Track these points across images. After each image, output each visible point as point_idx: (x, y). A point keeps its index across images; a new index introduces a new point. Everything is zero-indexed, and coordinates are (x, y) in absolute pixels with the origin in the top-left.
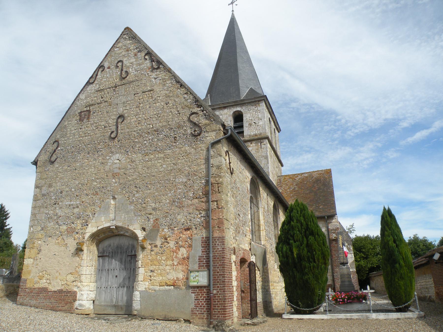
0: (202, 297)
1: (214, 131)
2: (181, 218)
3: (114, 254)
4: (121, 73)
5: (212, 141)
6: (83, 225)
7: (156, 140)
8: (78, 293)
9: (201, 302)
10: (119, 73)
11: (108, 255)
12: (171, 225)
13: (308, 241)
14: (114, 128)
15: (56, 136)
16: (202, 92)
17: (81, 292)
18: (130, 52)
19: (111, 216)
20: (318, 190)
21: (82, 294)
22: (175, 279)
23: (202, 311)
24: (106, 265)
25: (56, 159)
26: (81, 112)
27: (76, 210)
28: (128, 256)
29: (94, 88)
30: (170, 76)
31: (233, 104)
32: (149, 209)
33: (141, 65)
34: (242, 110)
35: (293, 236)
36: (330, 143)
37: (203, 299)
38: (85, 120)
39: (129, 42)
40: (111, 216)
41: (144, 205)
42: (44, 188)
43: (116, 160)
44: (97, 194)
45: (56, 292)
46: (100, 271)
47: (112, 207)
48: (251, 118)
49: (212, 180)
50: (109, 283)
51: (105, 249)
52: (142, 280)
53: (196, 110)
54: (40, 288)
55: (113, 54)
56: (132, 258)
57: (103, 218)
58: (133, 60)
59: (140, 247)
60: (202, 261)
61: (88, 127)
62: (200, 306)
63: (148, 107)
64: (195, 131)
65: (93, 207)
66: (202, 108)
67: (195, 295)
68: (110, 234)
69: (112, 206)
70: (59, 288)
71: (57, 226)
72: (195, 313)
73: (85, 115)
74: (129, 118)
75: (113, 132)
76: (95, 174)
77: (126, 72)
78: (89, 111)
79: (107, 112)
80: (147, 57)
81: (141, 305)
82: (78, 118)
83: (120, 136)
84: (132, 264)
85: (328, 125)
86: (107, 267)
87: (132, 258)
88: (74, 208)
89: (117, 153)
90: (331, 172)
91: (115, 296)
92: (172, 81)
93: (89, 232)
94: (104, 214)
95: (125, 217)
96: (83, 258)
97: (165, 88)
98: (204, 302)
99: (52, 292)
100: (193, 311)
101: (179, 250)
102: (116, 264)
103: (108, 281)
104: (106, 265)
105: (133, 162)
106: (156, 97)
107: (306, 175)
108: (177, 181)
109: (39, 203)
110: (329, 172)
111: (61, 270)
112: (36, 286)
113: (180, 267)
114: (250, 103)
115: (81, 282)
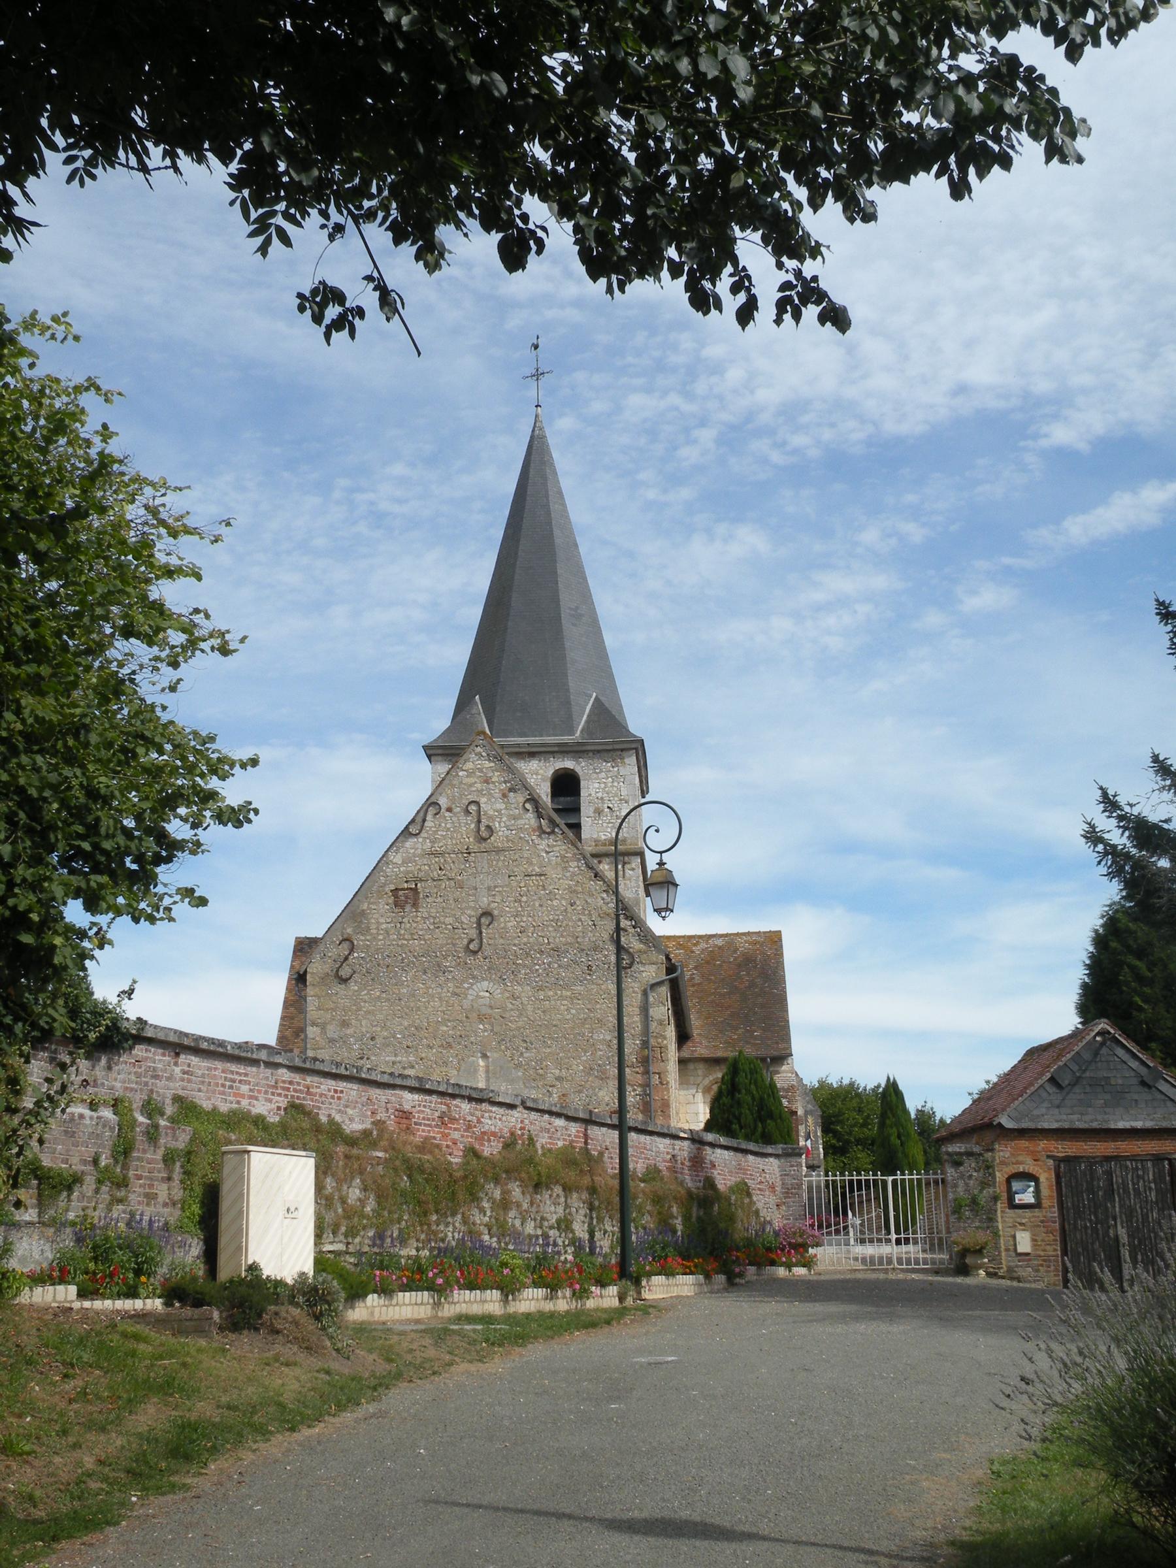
4: (479, 830)
10: (473, 826)
13: (764, 1128)
14: (473, 933)
18: (491, 786)
20: (749, 987)
29: (420, 846)
30: (575, 854)
31: (556, 749)
32: (550, 1078)
34: (578, 770)
35: (738, 1119)
36: (651, 494)
38: (408, 908)
39: (487, 764)
43: (483, 991)
44: (450, 1046)
48: (600, 795)
49: (652, 1042)
61: (418, 920)
63: (537, 904)
65: (444, 1069)
74: (502, 919)
75: (472, 941)
76: (443, 1012)
77: (488, 827)
78: (415, 890)
79: (456, 900)
82: (391, 900)
83: (488, 950)
85: (648, 390)
89: (483, 979)
90: (780, 940)
97: (568, 874)
105: (514, 997)
107: (720, 942)
108: (595, 1036)
110: (774, 939)
114: (599, 751)
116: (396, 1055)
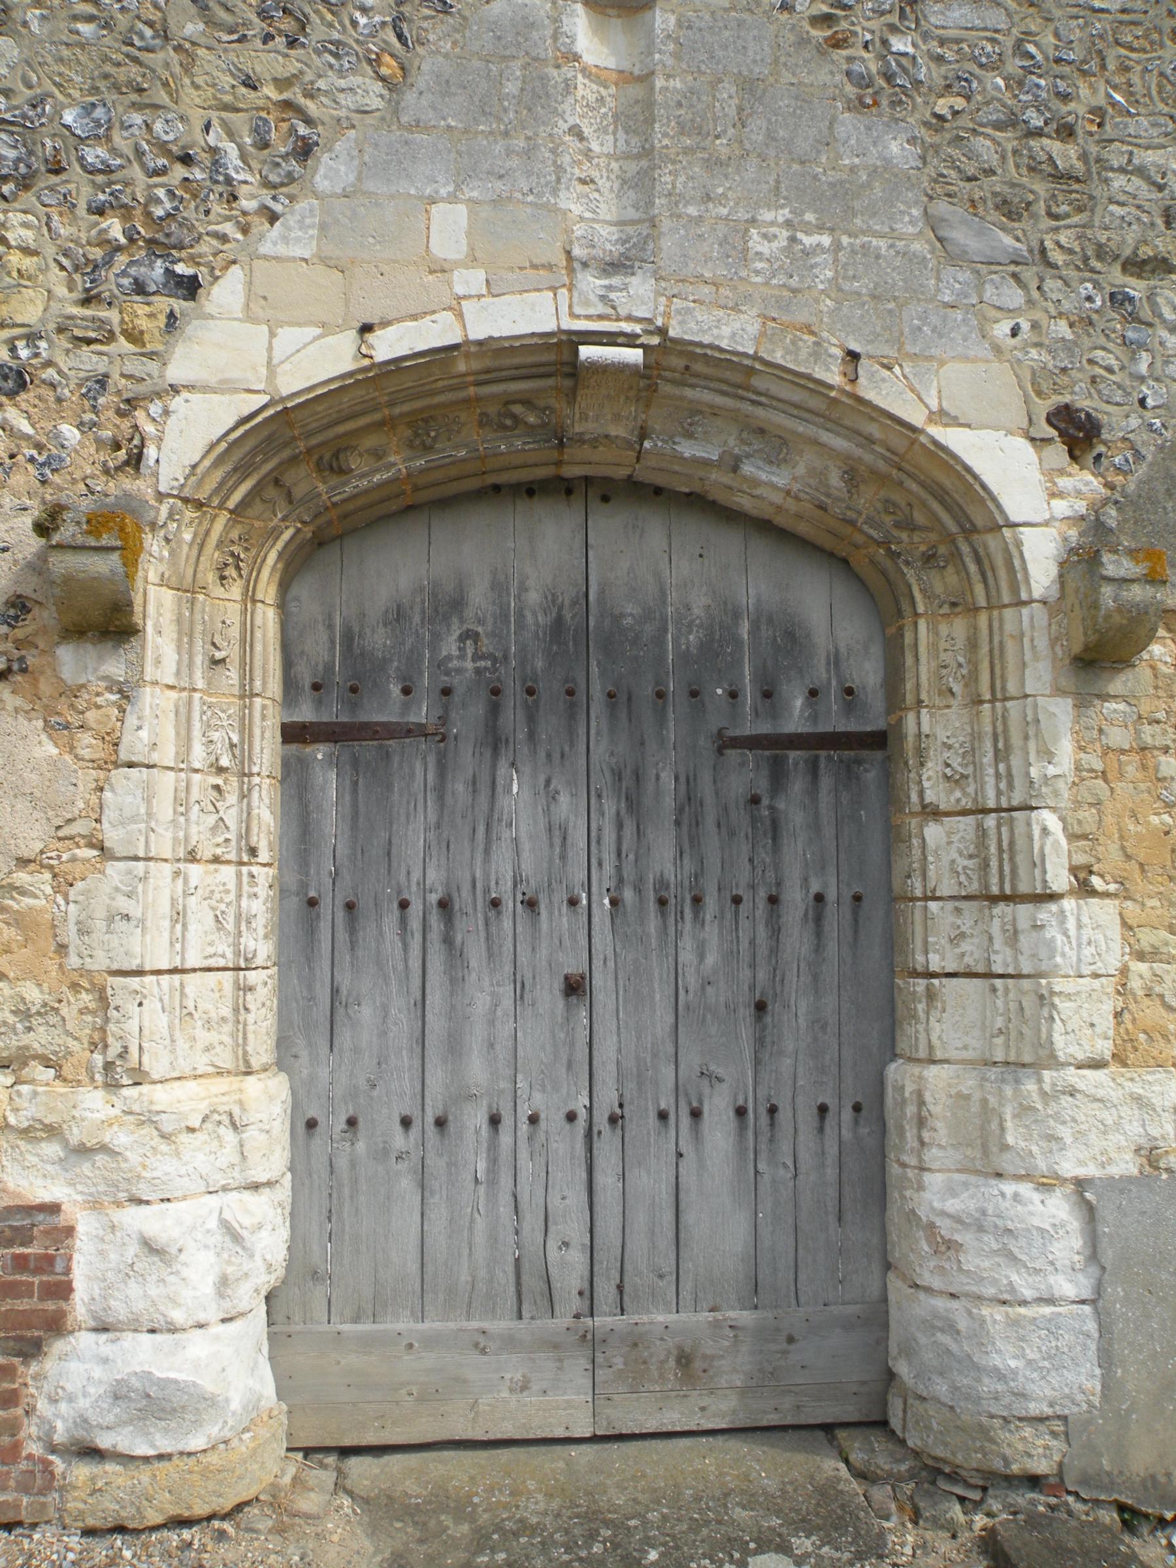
6: (111, 282)
8: (86, 1225)
11: (422, 713)
17: (134, 1219)
19: (571, 202)
21: (150, 1247)
24: (414, 837)
28: (725, 743)
40: (571, 202)
41: (1065, 154)
46: (322, 915)
47: (585, 107)
50: (477, 1071)
51: (378, 639)
52: (1105, 1048)
56: (778, 776)
57: (449, 228)
69: (585, 89)
81: (1106, 1358)
93: (225, 387)
94: (461, 178)
96: (136, 742)
102: (558, 834)
103: (455, 1048)
115: (119, 1072)
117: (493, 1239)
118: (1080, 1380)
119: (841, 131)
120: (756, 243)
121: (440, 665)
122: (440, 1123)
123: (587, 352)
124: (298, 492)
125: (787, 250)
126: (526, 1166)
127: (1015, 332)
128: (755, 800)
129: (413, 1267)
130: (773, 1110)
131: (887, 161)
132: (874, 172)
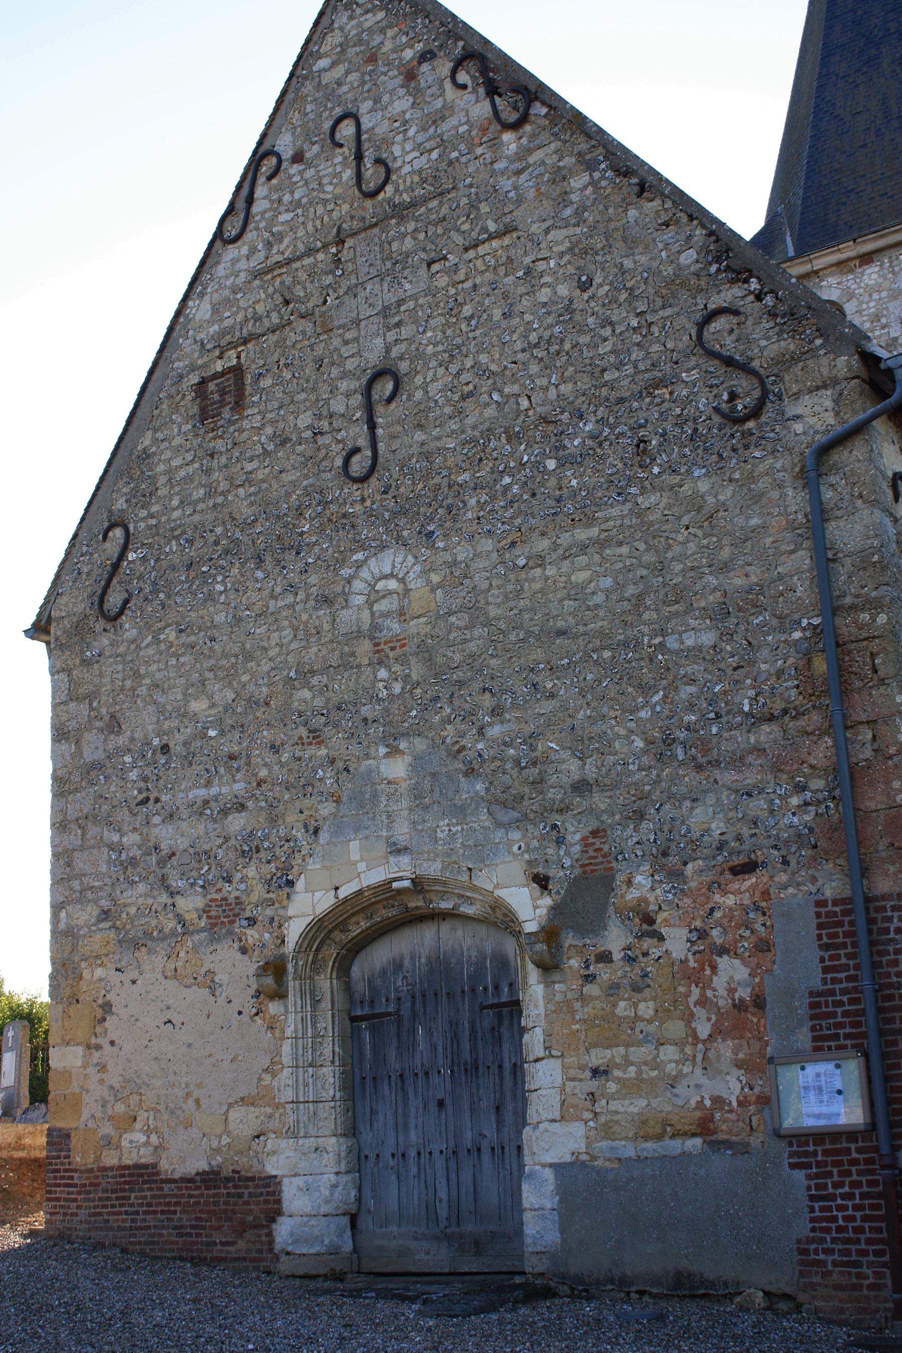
0: (841, 1185)
1: (825, 386)
2: (708, 819)
3: (419, 1005)
5: (821, 439)
7: (551, 464)
9: (841, 1208)
12: (665, 854)
14: (359, 435)
15: (113, 502)
16: (738, 191)
22: (708, 1103)
23: (848, 1253)
24: (392, 1053)
25: (126, 602)
26: (203, 382)
27: (237, 823)
33: (443, 119)
37: (850, 1196)
42: (88, 737)
45: (191, 1180)
50: (413, 1136)
51: (379, 982)
52: (559, 1118)
53: (729, 295)
54: (127, 1167)
55: (309, 87)
57: (355, 845)
58: (402, 104)
59: (530, 967)
60: (828, 1015)
62: (840, 1229)
63: (497, 314)
64: (733, 397)
66: (754, 284)
67: (809, 1177)
68: (391, 913)
70: (203, 1166)
71: (164, 898)
72: (817, 1263)
73: (223, 392)
77: (379, 161)
80: (463, 77)
84: (506, 1046)
86: (394, 1064)
87: (499, 1016)
88: (225, 812)
91: (443, 1194)
92: (597, 175)
93: (303, 915)
95: (452, 836)
97: (568, 212)
98: (856, 1208)
99: (173, 1181)
100: (804, 1252)
101: (714, 968)
104: (392, 1053)
106: (528, 260)
109: (82, 803)
111: (199, 1085)
112: (110, 1159)
113: (726, 1049)
116: (208, 784)
117: (419, 1198)
118: (553, 1237)
119: (461, 785)
120: (440, 835)
121: (396, 989)
122: (403, 1155)
123: (395, 885)
124: (337, 940)
125: (448, 835)
126: (429, 1171)
127: (520, 848)
128: (493, 1029)
129: (397, 1208)
130: (503, 1148)
131: (477, 792)
132: (472, 798)
